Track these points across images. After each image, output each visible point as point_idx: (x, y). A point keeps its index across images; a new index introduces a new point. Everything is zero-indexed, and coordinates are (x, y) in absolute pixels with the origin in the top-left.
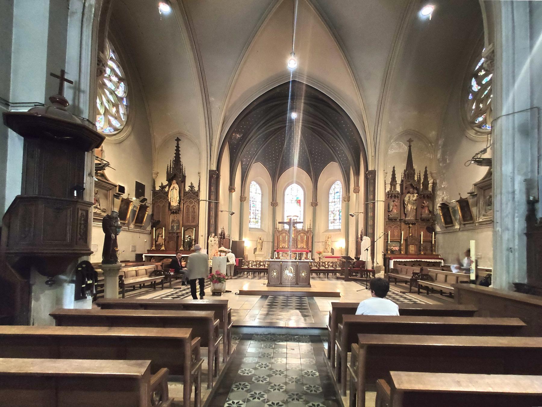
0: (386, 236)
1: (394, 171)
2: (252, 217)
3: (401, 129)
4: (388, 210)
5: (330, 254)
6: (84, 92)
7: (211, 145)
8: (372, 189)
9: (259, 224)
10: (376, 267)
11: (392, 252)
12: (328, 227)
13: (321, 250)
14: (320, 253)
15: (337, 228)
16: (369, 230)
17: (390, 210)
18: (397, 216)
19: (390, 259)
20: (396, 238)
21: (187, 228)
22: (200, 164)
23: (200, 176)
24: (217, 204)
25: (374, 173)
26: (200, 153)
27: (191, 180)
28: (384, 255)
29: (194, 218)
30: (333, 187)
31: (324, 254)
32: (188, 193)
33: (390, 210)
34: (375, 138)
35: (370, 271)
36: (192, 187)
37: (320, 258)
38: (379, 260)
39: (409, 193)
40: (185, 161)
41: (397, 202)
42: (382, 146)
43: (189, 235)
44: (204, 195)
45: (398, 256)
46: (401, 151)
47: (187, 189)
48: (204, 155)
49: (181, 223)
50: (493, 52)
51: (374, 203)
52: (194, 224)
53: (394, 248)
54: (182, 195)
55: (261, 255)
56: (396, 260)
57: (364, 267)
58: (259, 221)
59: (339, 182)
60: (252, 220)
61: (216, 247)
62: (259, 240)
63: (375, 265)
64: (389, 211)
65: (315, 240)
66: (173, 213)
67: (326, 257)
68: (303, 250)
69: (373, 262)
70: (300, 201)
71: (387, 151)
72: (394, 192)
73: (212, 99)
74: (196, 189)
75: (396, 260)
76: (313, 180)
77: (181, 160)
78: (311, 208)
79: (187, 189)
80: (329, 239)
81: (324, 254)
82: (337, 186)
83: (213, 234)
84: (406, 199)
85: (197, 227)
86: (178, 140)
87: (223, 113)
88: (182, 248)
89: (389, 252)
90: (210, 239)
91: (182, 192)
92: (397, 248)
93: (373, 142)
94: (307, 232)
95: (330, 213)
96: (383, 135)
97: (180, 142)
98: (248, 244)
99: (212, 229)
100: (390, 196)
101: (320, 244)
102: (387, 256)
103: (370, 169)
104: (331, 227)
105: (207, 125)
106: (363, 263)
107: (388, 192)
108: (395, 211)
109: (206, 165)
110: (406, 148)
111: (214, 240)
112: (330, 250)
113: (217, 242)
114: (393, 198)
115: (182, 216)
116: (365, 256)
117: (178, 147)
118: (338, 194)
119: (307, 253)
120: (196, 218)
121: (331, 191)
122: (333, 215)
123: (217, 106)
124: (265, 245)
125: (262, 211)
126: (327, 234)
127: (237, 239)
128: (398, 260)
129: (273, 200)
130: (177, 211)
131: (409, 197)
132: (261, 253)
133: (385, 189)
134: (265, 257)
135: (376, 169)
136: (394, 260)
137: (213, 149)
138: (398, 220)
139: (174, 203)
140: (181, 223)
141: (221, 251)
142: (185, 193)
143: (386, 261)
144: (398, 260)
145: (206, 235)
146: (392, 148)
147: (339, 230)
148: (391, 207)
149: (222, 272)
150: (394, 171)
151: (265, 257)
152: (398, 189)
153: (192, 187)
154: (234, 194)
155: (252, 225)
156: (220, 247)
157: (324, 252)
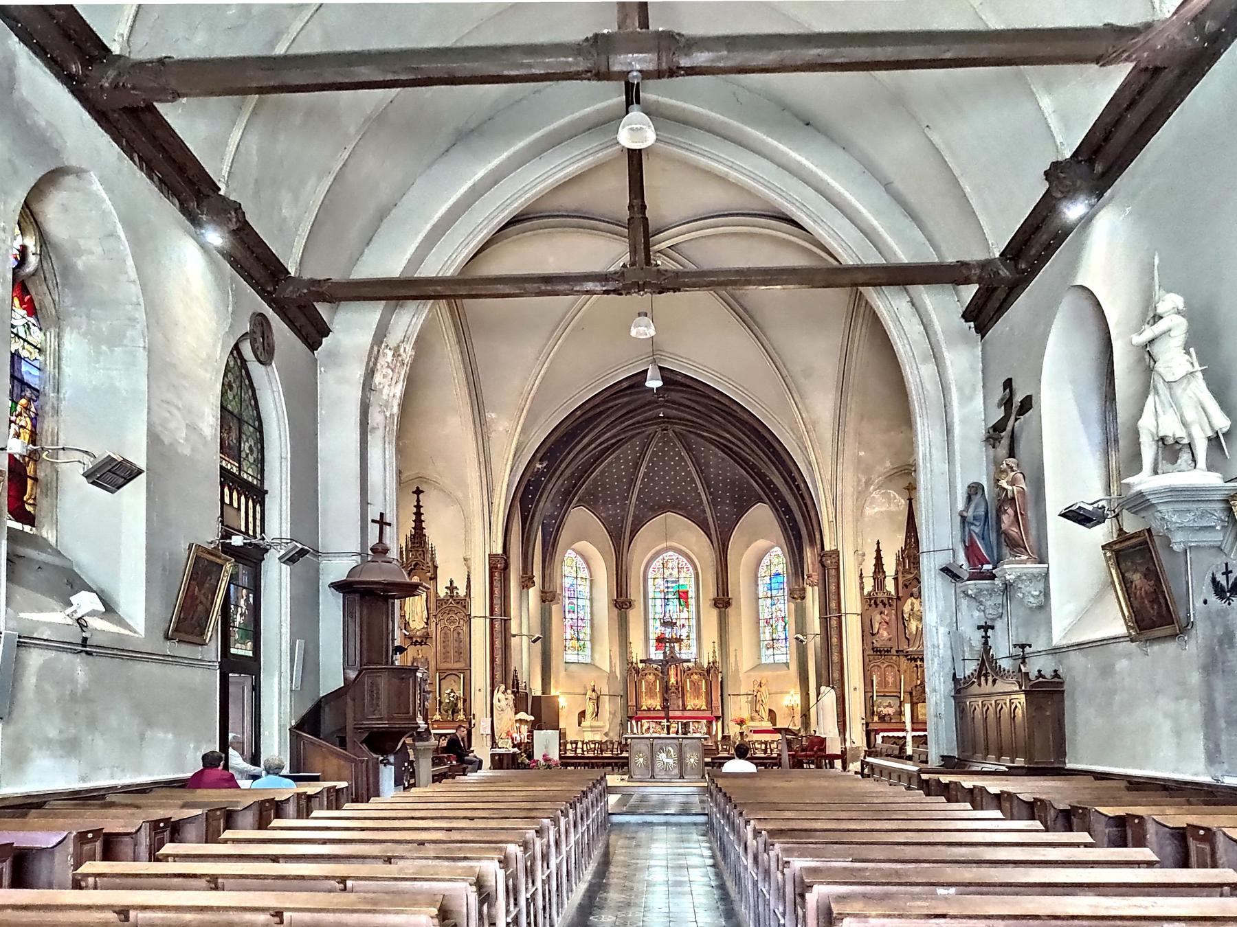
0: (868, 682)
1: (878, 551)
2: (569, 637)
4: (868, 632)
5: (767, 725)
7: (490, 504)
9: (588, 651)
10: (852, 749)
11: (882, 718)
12: (760, 658)
13: (745, 714)
14: (741, 722)
17: (875, 631)
18: (889, 644)
19: (877, 732)
20: (891, 689)
24: (506, 622)
30: (766, 561)
31: (752, 724)
32: (445, 601)
33: (875, 631)
34: (833, 485)
36: (452, 588)
37: (742, 734)
41: (890, 614)
42: (849, 504)
44: (479, 605)
46: (893, 508)
48: (477, 524)
49: (432, 664)
50: (857, 520)
53: (885, 711)
54: (432, 606)
55: (593, 729)
56: (886, 734)
57: (824, 750)
58: (588, 644)
59: (777, 550)
60: (569, 644)
61: (510, 712)
62: (589, 692)
63: (848, 744)
65: (729, 690)
67: (755, 732)
68: (700, 714)
70: (686, 593)
73: (490, 415)
74: (462, 592)
75: (886, 734)
76: (716, 544)
79: (442, 593)
80: (763, 689)
82: (775, 561)
83: (503, 687)
84: (907, 608)
85: (467, 670)
86: (418, 492)
89: (876, 719)
90: (497, 695)
91: (432, 599)
92: (891, 711)
94: (708, 671)
95: (762, 623)
98: (565, 699)
99: (498, 676)
100: (872, 602)
101: (743, 699)
102: (872, 727)
103: (827, 548)
104: (767, 657)
105: (483, 467)
107: (869, 594)
108: (885, 634)
109: (481, 545)
110: (903, 503)
111: (504, 699)
112: (765, 715)
113: (511, 703)
115: (433, 650)
116: (826, 727)
117: (418, 507)
118: (780, 579)
119: (710, 723)
120: (464, 652)
121: (761, 572)
126: (756, 675)
127: (538, 692)
128: (891, 734)
129: (619, 594)
131: (912, 604)
133: (862, 589)
134: (606, 734)
135: (840, 549)
136: (882, 734)
140: (432, 664)
141: (520, 721)
142: (438, 600)
144: (891, 734)
145: (489, 689)
146: (871, 503)
147: (787, 664)
148: (876, 626)
149: (550, 756)
150: (878, 551)
151: (606, 734)
152: (890, 586)
153: (452, 588)
154: (531, 590)
155: (571, 657)
157: (752, 719)
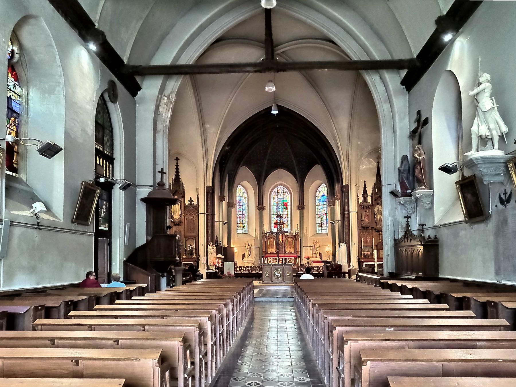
0: (360, 241)
1: (365, 185)
3: (370, 148)
4: (360, 220)
5: (318, 259)
6: (165, 173)
7: (207, 164)
8: (346, 201)
9: (246, 228)
10: (352, 269)
11: (365, 256)
13: (310, 255)
14: (308, 258)
15: (325, 231)
16: (345, 238)
18: (369, 225)
19: (363, 262)
20: (369, 244)
21: (189, 238)
22: (197, 181)
23: (198, 192)
25: (348, 186)
26: (197, 171)
27: (190, 195)
28: (359, 259)
29: (194, 229)
30: (319, 189)
31: (312, 259)
34: (347, 157)
35: (347, 273)
36: (191, 201)
38: (355, 264)
39: (378, 204)
40: (184, 179)
43: (190, 245)
44: (202, 208)
45: (369, 260)
46: (371, 166)
47: (187, 203)
51: (349, 214)
52: (194, 234)
55: (248, 261)
56: (366, 263)
58: (246, 225)
61: (214, 254)
62: (247, 246)
63: (351, 268)
64: (362, 221)
65: (304, 244)
66: (176, 225)
69: (350, 266)
70: (287, 203)
71: (359, 167)
72: (365, 204)
73: (208, 126)
74: (195, 203)
75: (366, 263)
77: (181, 177)
78: (298, 211)
79: (187, 203)
80: (317, 244)
81: (312, 259)
82: (323, 189)
83: (212, 244)
84: (376, 209)
86: (177, 159)
87: (217, 139)
88: (185, 256)
89: (363, 257)
90: (209, 247)
92: (369, 253)
93: (345, 160)
95: (317, 216)
96: (353, 158)
97: (178, 161)
100: (363, 207)
103: (344, 184)
104: (319, 230)
106: (341, 266)
108: (367, 220)
110: (375, 164)
111: (212, 249)
112: (318, 255)
113: (215, 250)
114: (365, 209)
116: (342, 260)
117: (177, 166)
118: (325, 197)
119: (295, 259)
120: (196, 228)
122: (319, 219)
123: (212, 132)
124: (253, 251)
125: (248, 215)
127: (226, 246)
128: (368, 263)
130: (178, 223)
131: (378, 208)
132: (249, 259)
133: (358, 201)
136: (365, 263)
137: (209, 167)
138: (370, 228)
139: (177, 217)
142: (186, 206)
143: (360, 263)
144: (368, 263)
150: (365, 185)
152: (369, 200)
153: (191, 201)
154: (224, 202)
156: (217, 255)
157: (313, 257)
